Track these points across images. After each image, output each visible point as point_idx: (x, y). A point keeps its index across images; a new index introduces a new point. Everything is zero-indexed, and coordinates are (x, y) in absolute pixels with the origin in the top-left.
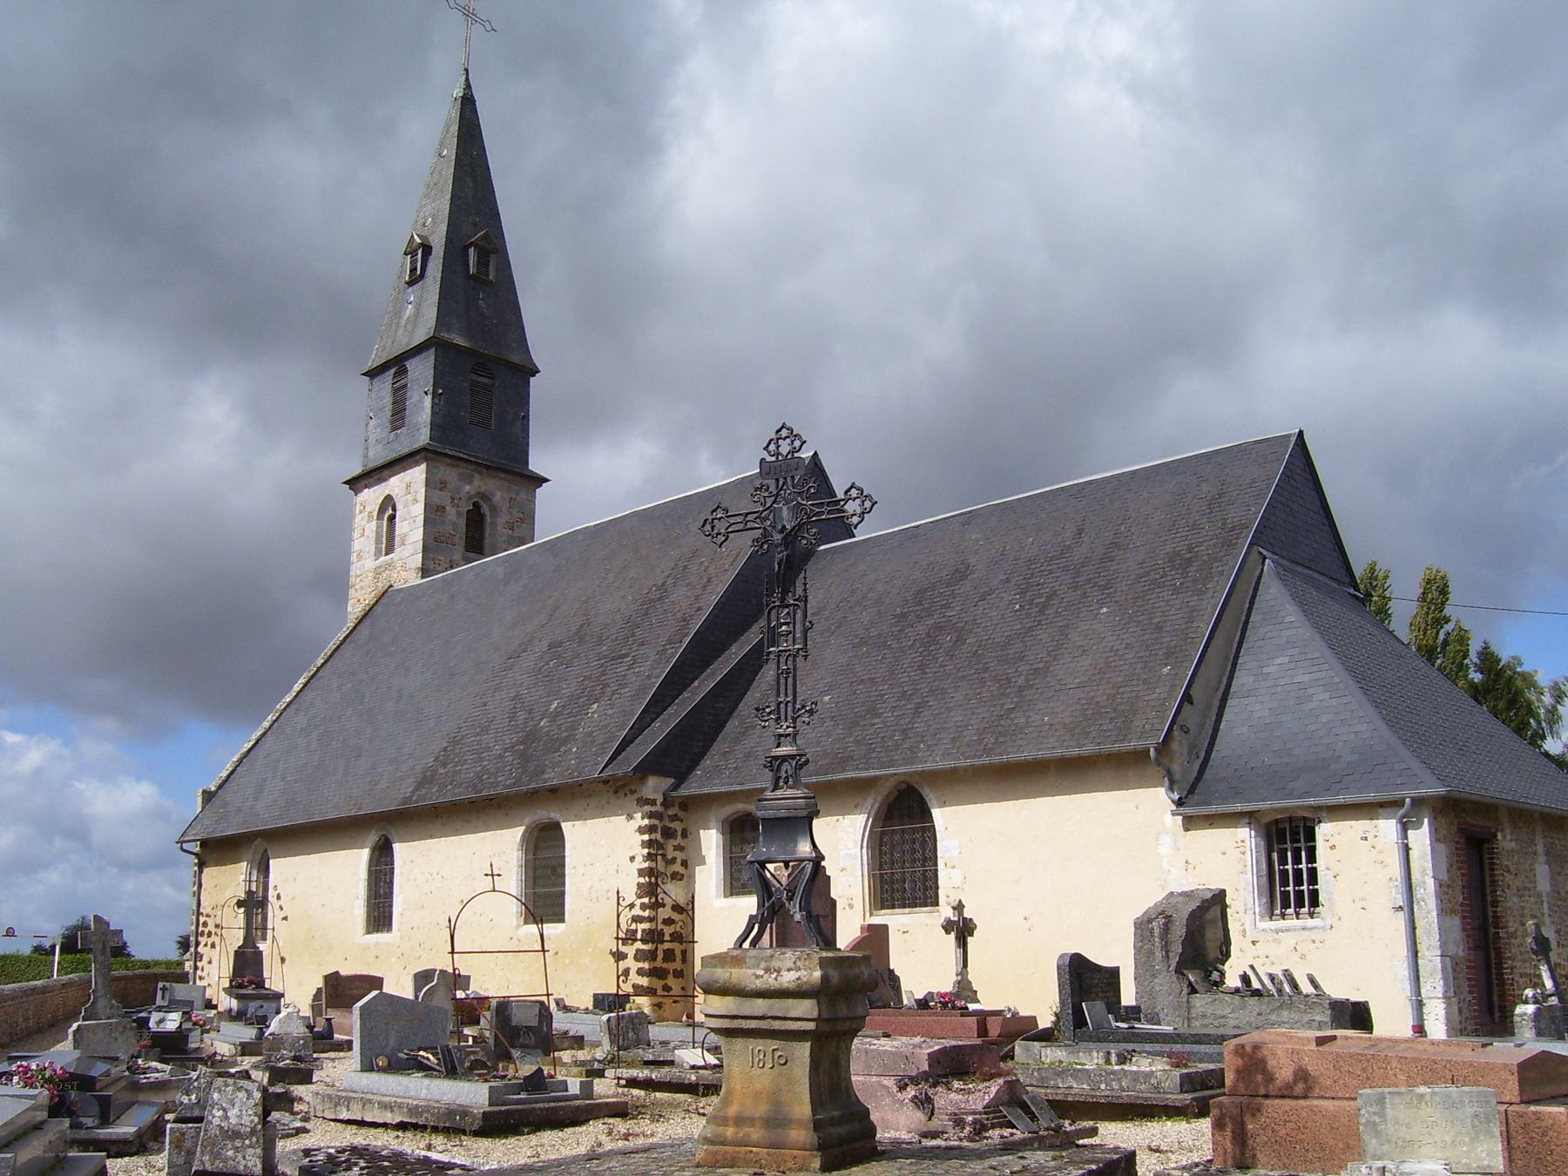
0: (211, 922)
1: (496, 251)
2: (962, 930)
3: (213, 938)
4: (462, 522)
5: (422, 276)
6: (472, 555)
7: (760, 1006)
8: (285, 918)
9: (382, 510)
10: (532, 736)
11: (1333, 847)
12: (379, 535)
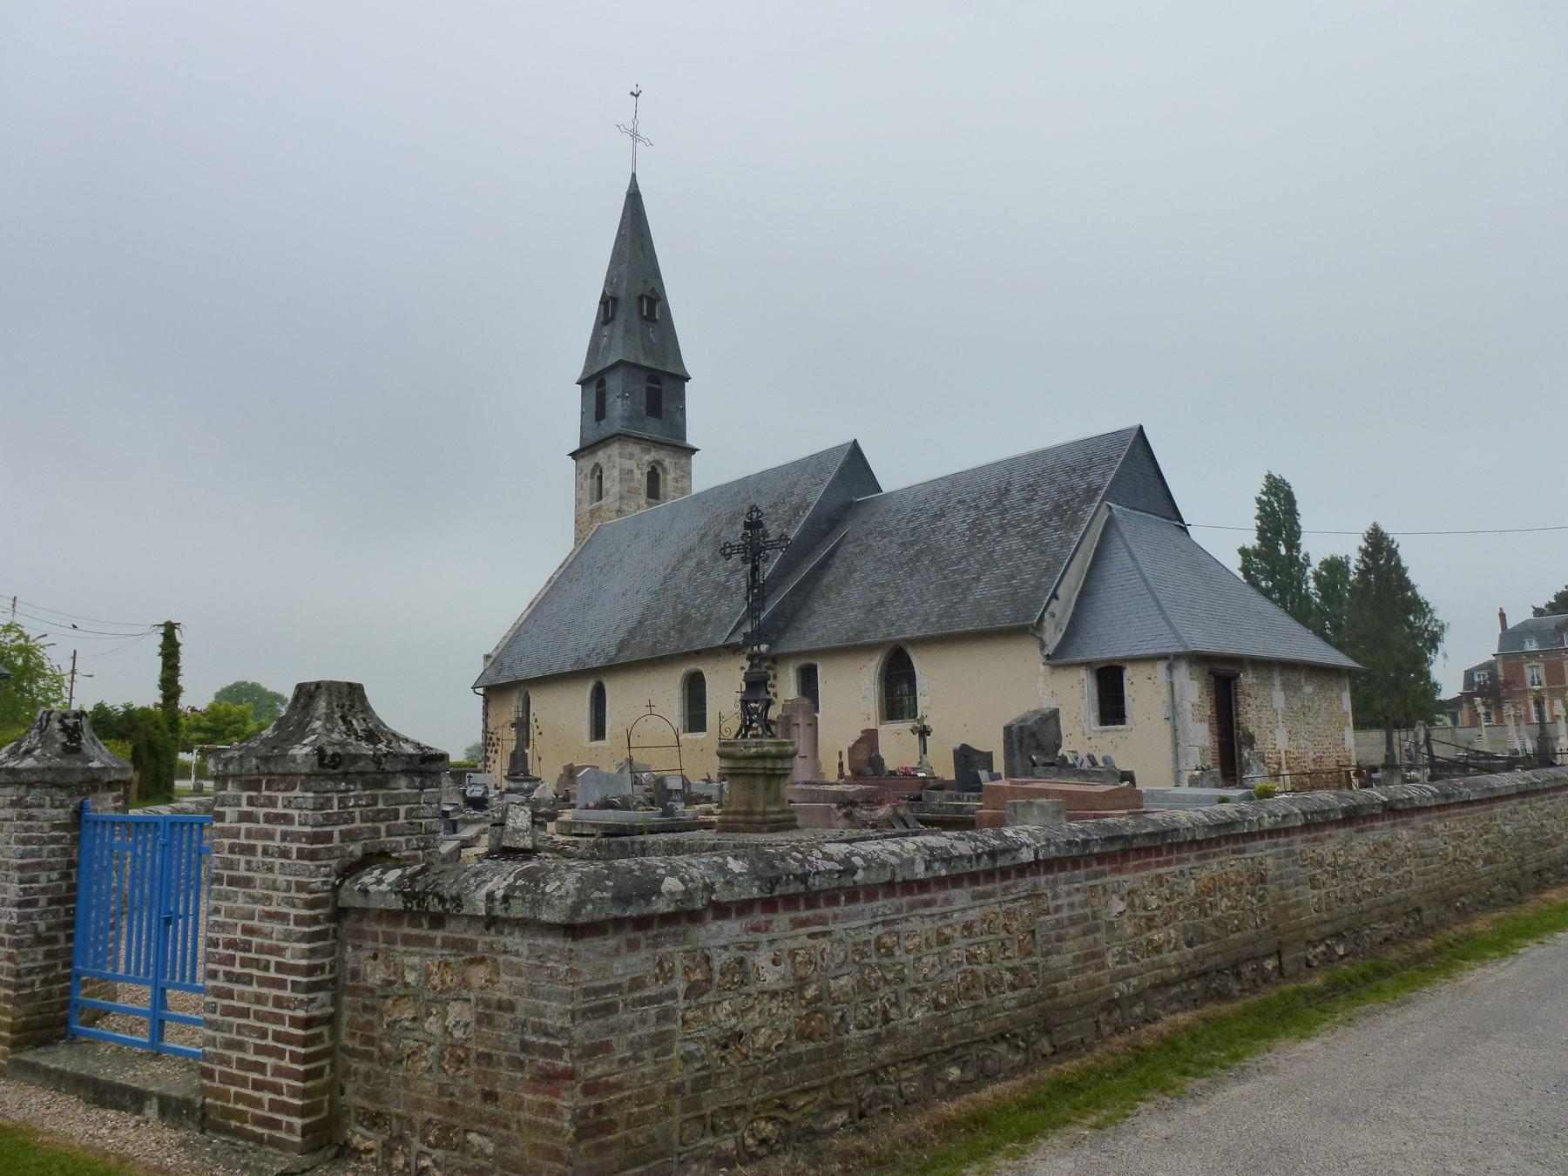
0: (494, 737)
1: (659, 300)
2: (924, 732)
3: (496, 747)
4: (645, 479)
5: (612, 319)
6: (652, 500)
7: (742, 764)
8: (540, 734)
9: (593, 472)
10: (686, 618)
11: (1132, 683)
12: (592, 489)
